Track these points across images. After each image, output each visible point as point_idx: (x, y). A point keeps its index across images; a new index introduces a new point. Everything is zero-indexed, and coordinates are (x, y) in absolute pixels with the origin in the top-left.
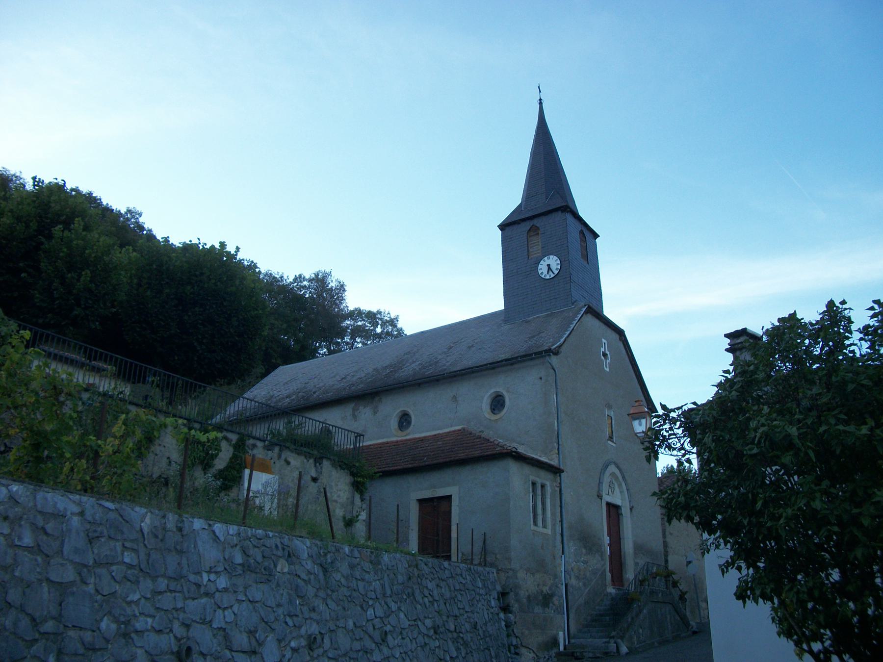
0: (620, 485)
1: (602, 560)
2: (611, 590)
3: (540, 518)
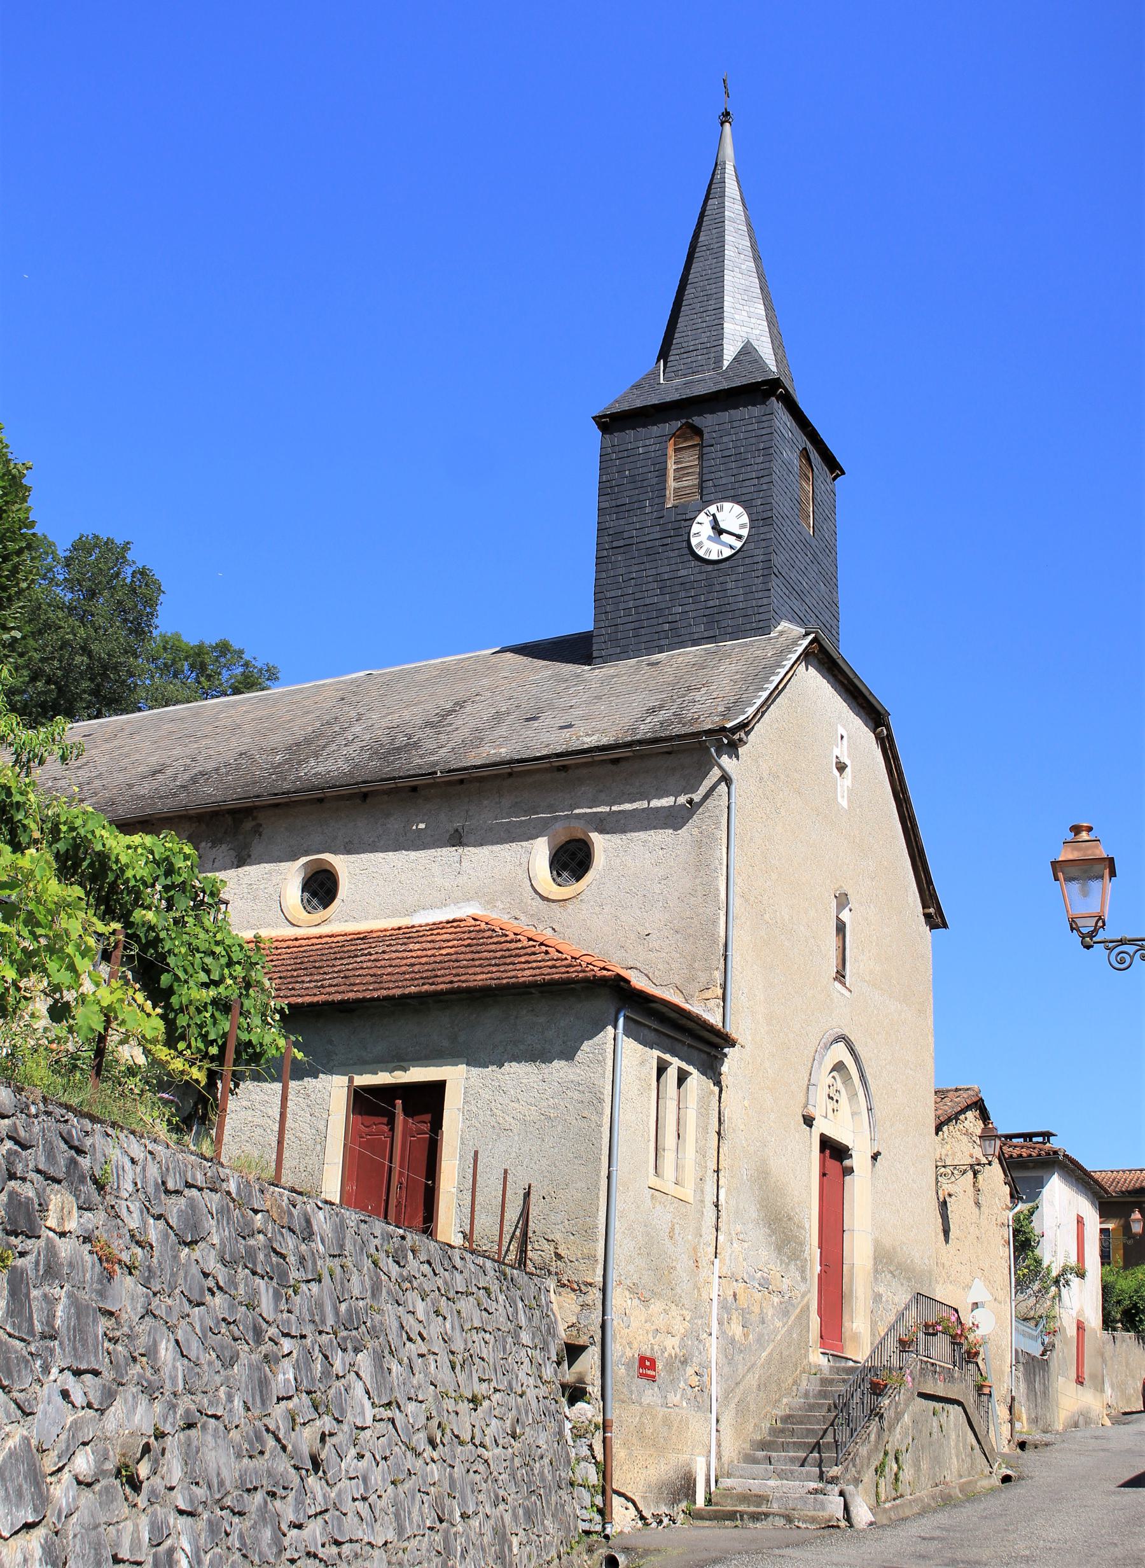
0: (853, 1096)
1: (804, 1279)
2: (818, 1359)
3: (669, 1158)
